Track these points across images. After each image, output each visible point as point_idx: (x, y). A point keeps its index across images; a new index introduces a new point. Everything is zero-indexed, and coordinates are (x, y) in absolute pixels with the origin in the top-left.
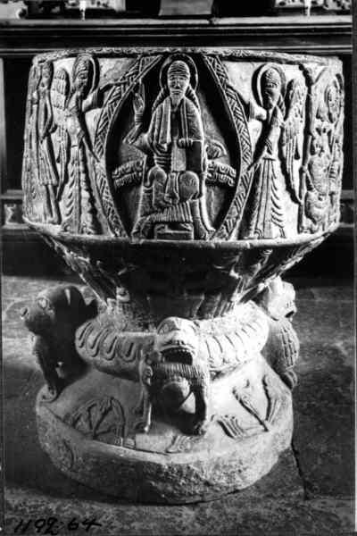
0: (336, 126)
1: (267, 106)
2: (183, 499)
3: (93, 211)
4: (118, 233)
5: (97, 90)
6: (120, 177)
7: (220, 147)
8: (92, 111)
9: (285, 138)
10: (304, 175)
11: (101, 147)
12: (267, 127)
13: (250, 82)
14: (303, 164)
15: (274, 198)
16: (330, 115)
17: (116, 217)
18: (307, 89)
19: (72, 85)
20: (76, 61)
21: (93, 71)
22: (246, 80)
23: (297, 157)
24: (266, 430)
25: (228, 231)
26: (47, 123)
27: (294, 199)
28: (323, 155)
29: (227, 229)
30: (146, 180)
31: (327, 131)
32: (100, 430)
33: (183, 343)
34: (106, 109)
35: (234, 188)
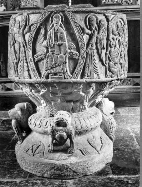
0: (122, 38)
1: (91, 29)
2: (65, 177)
3: (28, 70)
4: (37, 78)
5: (28, 26)
6: (37, 57)
7: (73, 45)
8: (27, 34)
9: (98, 41)
10: (107, 55)
11: (30, 47)
12: (91, 37)
13: (84, 20)
14: (107, 51)
15: (94, 63)
16: (119, 34)
17: (36, 72)
18: (107, 23)
19: (21, 25)
20: (22, 16)
21: (27, 20)
22: (82, 20)
23: (104, 48)
24: (99, 154)
25: (77, 76)
26: (13, 40)
27: (103, 64)
28: (116, 48)
29: (76, 75)
30: (46, 58)
31: (118, 39)
32: (36, 153)
33: (63, 118)
34: (32, 33)
35: (78, 60)
